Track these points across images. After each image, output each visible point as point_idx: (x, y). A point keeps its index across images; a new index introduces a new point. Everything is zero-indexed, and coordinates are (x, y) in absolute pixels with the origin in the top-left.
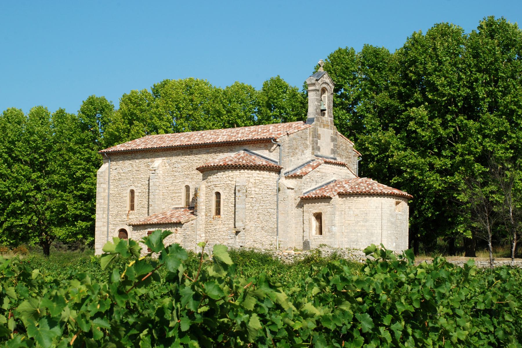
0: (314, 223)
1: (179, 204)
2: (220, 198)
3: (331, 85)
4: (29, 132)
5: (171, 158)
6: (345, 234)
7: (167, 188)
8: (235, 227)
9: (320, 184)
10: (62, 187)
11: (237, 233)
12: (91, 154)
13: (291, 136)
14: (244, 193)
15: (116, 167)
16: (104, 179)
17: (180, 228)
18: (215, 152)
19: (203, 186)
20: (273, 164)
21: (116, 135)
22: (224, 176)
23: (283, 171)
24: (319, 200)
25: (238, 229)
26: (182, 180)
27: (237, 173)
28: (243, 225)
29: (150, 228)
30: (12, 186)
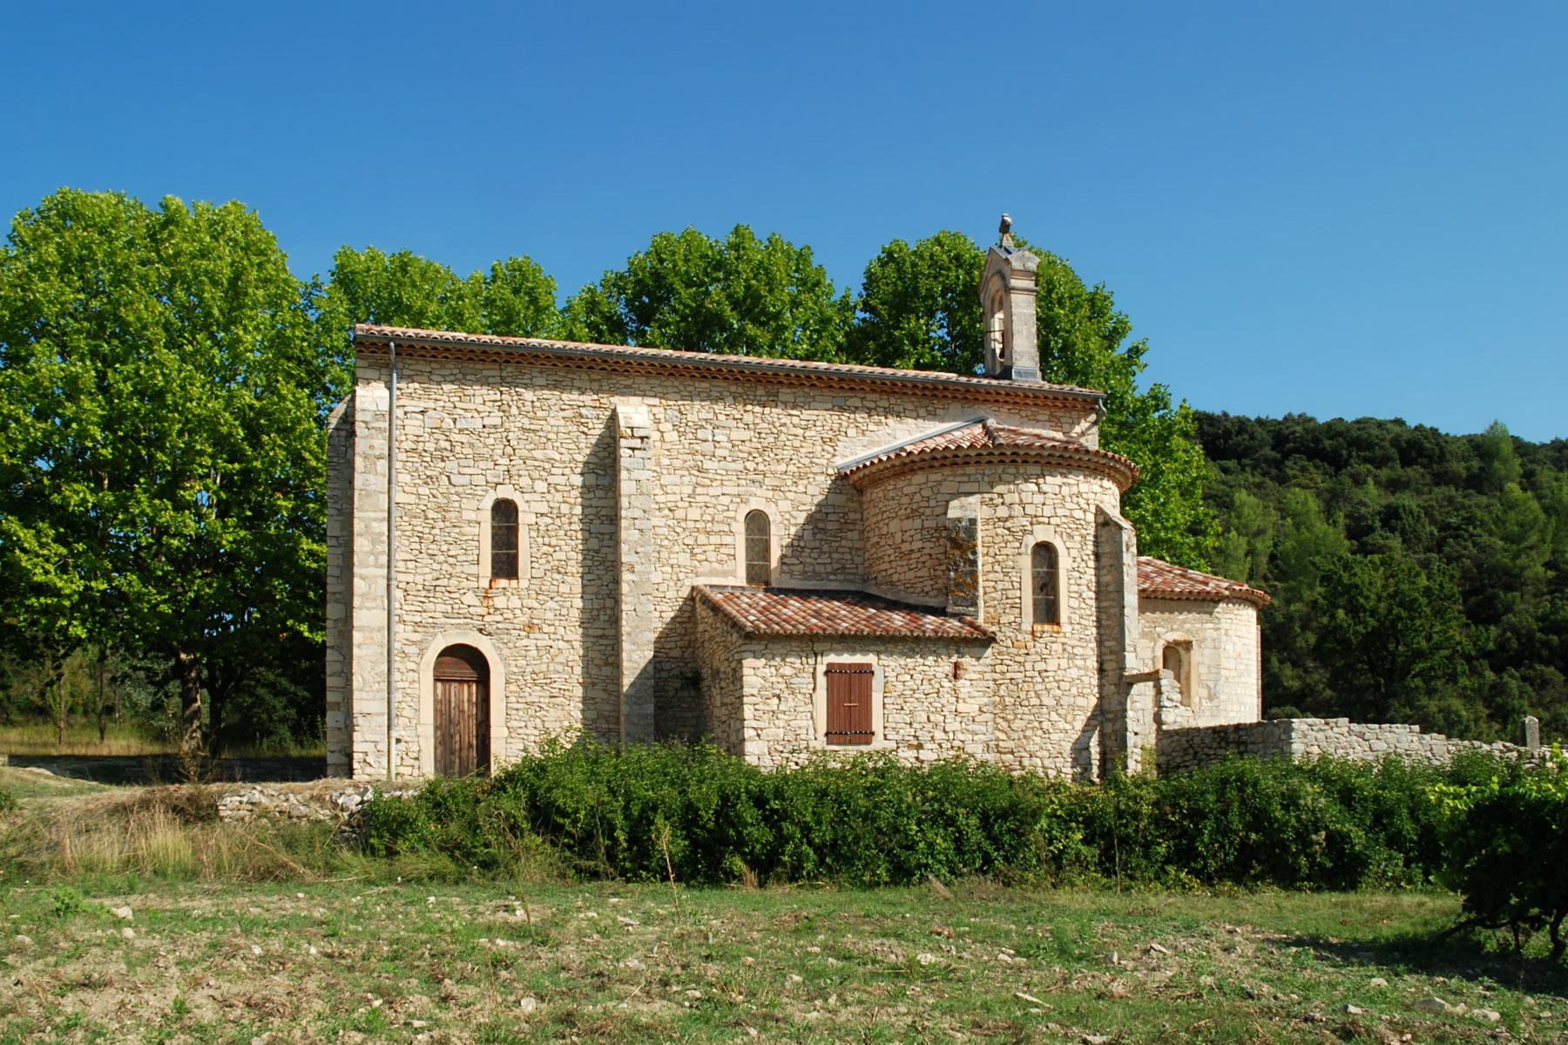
1: (725, 574)
7: (666, 512)
15: (422, 405)
17: (973, 661)
18: (869, 412)
24: (1181, 603)
26: (735, 491)
29: (839, 652)
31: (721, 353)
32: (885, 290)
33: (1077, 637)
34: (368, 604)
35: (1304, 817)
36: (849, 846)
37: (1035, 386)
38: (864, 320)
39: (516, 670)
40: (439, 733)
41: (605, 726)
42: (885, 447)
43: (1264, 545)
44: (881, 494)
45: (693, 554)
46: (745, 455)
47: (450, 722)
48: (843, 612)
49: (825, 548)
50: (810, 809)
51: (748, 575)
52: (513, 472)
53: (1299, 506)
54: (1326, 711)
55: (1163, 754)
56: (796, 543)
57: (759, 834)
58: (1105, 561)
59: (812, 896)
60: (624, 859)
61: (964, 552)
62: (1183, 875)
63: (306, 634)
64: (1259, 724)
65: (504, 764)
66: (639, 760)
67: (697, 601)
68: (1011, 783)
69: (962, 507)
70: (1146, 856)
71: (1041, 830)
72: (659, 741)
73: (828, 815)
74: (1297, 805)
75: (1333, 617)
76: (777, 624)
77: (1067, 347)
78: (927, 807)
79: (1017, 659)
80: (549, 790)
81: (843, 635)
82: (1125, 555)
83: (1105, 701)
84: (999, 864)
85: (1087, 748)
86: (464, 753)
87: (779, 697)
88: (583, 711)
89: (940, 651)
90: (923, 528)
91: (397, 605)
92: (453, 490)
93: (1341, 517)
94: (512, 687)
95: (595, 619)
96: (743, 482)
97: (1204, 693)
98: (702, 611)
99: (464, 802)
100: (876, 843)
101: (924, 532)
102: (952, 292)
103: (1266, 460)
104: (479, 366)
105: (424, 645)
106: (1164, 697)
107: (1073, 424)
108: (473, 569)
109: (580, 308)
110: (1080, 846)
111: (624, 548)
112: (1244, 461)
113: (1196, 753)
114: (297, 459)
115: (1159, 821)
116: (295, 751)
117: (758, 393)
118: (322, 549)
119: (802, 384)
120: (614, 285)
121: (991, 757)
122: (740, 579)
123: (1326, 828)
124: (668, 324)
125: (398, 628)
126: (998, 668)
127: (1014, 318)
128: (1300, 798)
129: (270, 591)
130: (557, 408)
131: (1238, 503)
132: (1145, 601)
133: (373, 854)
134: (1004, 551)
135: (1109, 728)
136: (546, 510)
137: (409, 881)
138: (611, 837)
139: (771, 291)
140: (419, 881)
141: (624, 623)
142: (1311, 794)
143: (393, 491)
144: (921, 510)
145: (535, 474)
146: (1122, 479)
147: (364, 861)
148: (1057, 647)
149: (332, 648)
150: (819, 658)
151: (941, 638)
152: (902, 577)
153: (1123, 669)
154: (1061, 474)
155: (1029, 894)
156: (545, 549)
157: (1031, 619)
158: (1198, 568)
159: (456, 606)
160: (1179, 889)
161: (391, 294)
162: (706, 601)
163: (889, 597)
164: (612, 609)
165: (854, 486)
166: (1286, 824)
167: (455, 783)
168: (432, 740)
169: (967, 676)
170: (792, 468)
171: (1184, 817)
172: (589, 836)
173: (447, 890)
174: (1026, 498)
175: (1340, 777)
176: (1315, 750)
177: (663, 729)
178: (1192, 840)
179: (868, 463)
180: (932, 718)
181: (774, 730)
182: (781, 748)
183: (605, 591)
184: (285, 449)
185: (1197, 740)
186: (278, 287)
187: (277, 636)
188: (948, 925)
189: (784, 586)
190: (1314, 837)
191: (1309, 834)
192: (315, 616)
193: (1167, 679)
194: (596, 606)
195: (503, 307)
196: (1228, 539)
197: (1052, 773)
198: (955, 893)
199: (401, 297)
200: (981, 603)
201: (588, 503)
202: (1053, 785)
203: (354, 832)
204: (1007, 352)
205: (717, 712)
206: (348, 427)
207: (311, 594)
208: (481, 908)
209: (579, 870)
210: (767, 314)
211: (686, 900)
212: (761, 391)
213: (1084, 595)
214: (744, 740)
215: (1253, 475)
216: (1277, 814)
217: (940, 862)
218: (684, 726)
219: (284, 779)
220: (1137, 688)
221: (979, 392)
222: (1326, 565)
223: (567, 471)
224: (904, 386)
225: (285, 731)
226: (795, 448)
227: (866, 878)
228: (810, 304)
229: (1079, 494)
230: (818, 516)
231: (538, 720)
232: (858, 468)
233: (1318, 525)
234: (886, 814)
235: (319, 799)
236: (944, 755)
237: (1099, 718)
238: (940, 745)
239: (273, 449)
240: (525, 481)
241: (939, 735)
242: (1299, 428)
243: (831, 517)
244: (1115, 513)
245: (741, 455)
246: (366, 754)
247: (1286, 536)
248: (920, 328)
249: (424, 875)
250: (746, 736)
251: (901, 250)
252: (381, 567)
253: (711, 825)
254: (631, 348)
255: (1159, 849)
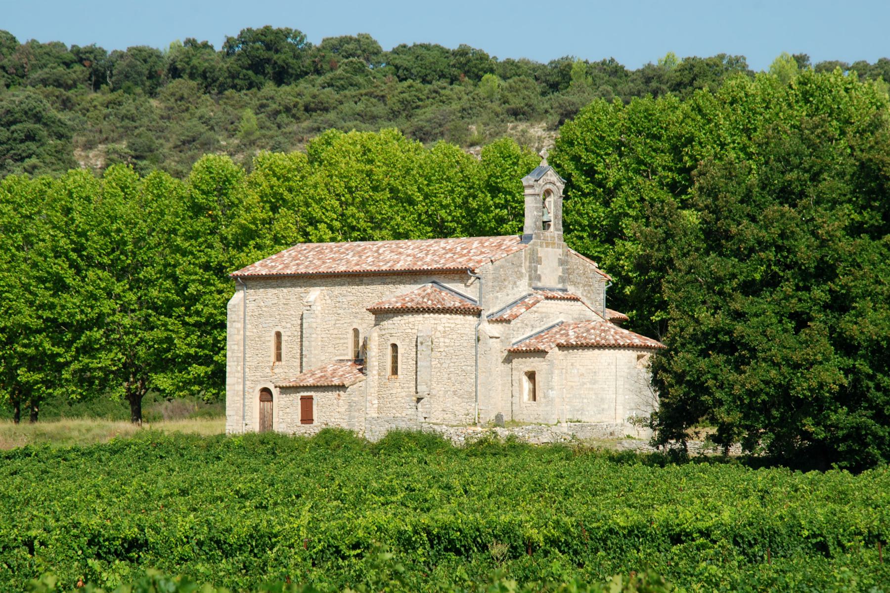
0: (526, 384)
1: (345, 355)
2: (397, 352)
3: (559, 184)
4: (109, 217)
5: (333, 288)
6: (567, 400)
8: (417, 393)
9: (538, 330)
10: (168, 309)
11: (419, 400)
12: (210, 256)
13: (497, 263)
14: (428, 346)
16: (238, 315)
18: (394, 283)
19: (375, 335)
20: (469, 304)
21: (251, 230)
22: (402, 322)
23: (484, 314)
25: (420, 395)
27: (419, 317)
28: (428, 389)
30: (85, 305)
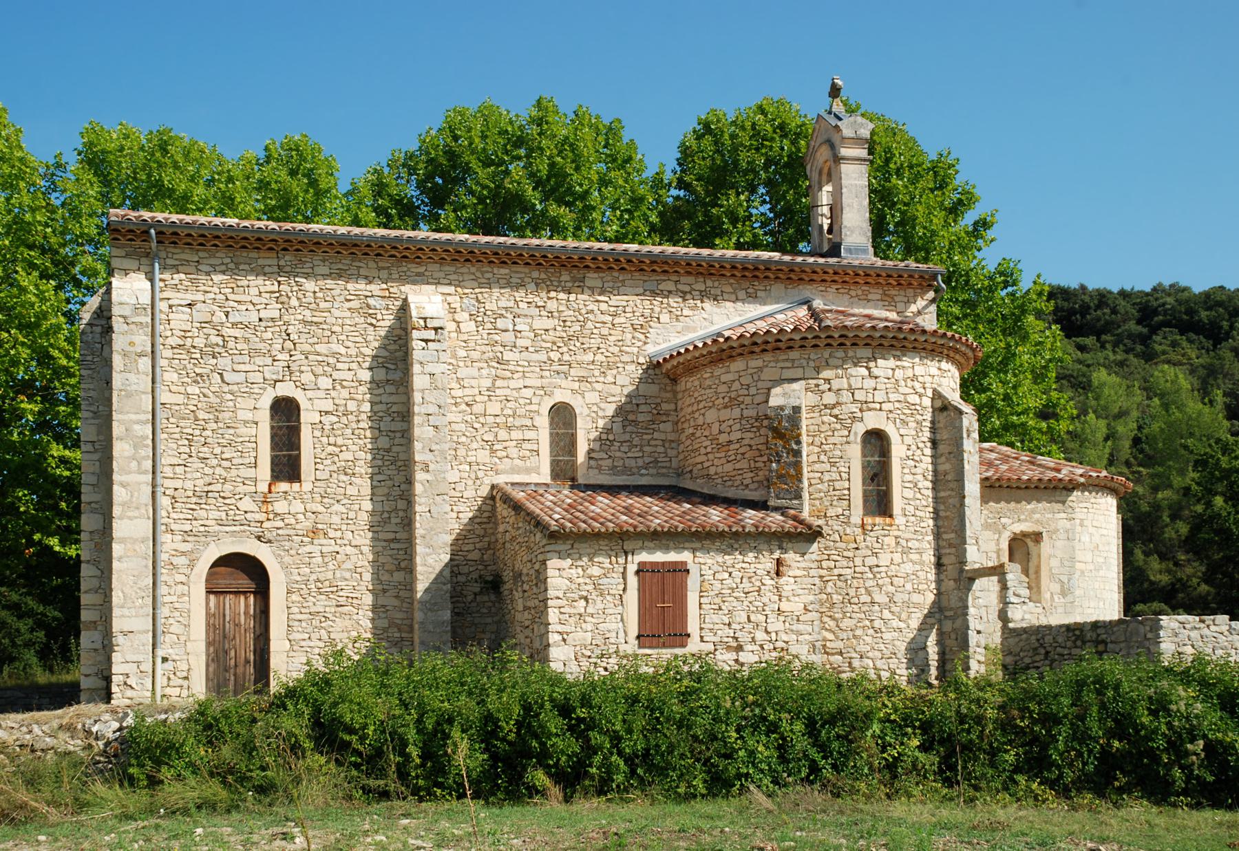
1: (528, 471)
7: (464, 407)
15: (189, 297)
17: (797, 557)
18: (684, 295)
22: (899, 374)
24: (1029, 492)
26: (538, 383)
29: (651, 550)
31: (523, 237)
32: (701, 165)
33: (912, 529)
34: (129, 514)
35: (1176, 723)
36: (662, 755)
37: (866, 263)
38: (677, 198)
39: (298, 578)
40: (212, 649)
41: (397, 635)
42: (701, 333)
43: (1126, 429)
44: (697, 383)
45: (493, 451)
46: (549, 345)
47: (225, 637)
48: (656, 508)
49: (636, 441)
50: (620, 717)
51: (552, 471)
52: (294, 367)
53: (1168, 385)
54: (1200, 607)
55: (1011, 653)
56: (604, 437)
57: (564, 746)
58: (942, 448)
59: (623, 811)
60: (417, 777)
61: (787, 442)
62: (1035, 786)
63: (57, 549)
64: (1120, 621)
65: (284, 680)
66: (433, 670)
67: (497, 499)
68: (839, 686)
69: (784, 394)
70: (993, 765)
71: (873, 736)
72: (455, 648)
73: (639, 723)
74: (1168, 712)
75: (1209, 504)
76: (584, 522)
77: (906, 222)
78: (747, 712)
79: (845, 554)
80: (335, 704)
81: (655, 533)
82: (965, 442)
83: (944, 598)
84: (828, 773)
85: (924, 648)
86: (240, 670)
87: (586, 599)
88: (373, 620)
89: (761, 547)
90: (742, 417)
91: (164, 513)
92: (226, 389)
93: (1219, 396)
94: (295, 597)
95: (386, 521)
96: (547, 373)
97: (1056, 587)
98: (502, 510)
99: (239, 722)
100: (692, 752)
101: (744, 422)
102: (776, 164)
103: (1131, 336)
104: (254, 254)
105: (194, 556)
106: (1010, 592)
107: (908, 302)
108: (251, 473)
109: (366, 192)
110: (917, 753)
111: (417, 446)
112: (1104, 337)
113: (1047, 653)
114: (44, 358)
115: (1005, 726)
116: (42, 677)
117: (563, 278)
118: (74, 455)
119: (611, 268)
120: (404, 165)
121: (817, 659)
122: (545, 476)
123: (1205, 737)
124: (464, 207)
125: (165, 538)
126: (825, 564)
127: (844, 190)
128: (1171, 702)
129: (13, 503)
130: (342, 298)
131: (1096, 383)
132: (988, 489)
133: (131, 785)
134: (831, 440)
135: (948, 626)
136: (331, 408)
137: (174, 813)
138: (403, 753)
139: (577, 169)
140: (185, 812)
141: (418, 525)
142: (1183, 698)
143: (158, 391)
144: (741, 399)
145: (319, 370)
146: (963, 361)
147: (120, 792)
148: (890, 541)
149: (88, 562)
150: (630, 558)
151: (762, 534)
152: (720, 469)
153: (963, 562)
154: (894, 357)
155: (861, 806)
156: (330, 449)
157: (861, 512)
158: (1049, 454)
159: (231, 513)
160: (1031, 801)
161: (149, 175)
162: (507, 499)
163: (705, 491)
164: (405, 511)
165: (667, 375)
166: (1155, 731)
167: (229, 703)
168: (204, 658)
169: (791, 573)
170: (599, 357)
171: (1034, 722)
172: (379, 753)
173: (217, 820)
174: (856, 383)
175: (1220, 681)
176: (1189, 650)
177: (462, 632)
178: (1044, 748)
179: (682, 351)
180: (752, 618)
181: (581, 634)
182: (589, 653)
183: (396, 491)
184: (29, 347)
185: (1048, 639)
186: (13, 167)
187: (23, 553)
188: (771, 840)
189: (592, 482)
190: (1189, 746)
191: (1183, 742)
192: (68, 528)
193: (1014, 574)
194: (387, 508)
195: (279, 190)
196: (1085, 421)
197: (885, 675)
198: (779, 805)
199: (161, 180)
200: (806, 495)
201: (377, 399)
202: (885, 687)
203: (110, 762)
204: (835, 228)
205: (519, 617)
206: (103, 322)
207: (63, 505)
208: (255, 838)
209: (366, 790)
210: (573, 194)
211: (485, 819)
212: (565, 277)
213: (920, 485)
214: (549, 645)
215: (1114, 352)
216: (1144, 720)
217: (762, 771)
218: (483, 632)
219: (28, 709)
220: (979, 584)
221: (804, 271)
222: (1202, 449)
223: (354, 366)
224: (722, 267)
225: (31, 657)
226: (603, 336)
227: (681, 790)
228: (621, 182)
229: (914, 378)
230: (628, 407)
231: (323, 631)
232: (672, 356)
233: (1191, 404)
234: (702, 722)
235: (70, 728)
236: (766, 657)
237: (937, 616)
238: (762, 647)
239: (14, 347)
240: (307, 378)
241: (760, 636)
242: (1169, 300)
243: (642, 408)
244: (954, 397)
245: (544, 345)
246: (127, 675)
247: (1153, 417)
248: (741, 205)
249: (191, 805)
250: (551, 641)
251: (718, 121)
252: (145, 472)
253: (512, 736)
254: (423, 233)
255: (1007, 757)
